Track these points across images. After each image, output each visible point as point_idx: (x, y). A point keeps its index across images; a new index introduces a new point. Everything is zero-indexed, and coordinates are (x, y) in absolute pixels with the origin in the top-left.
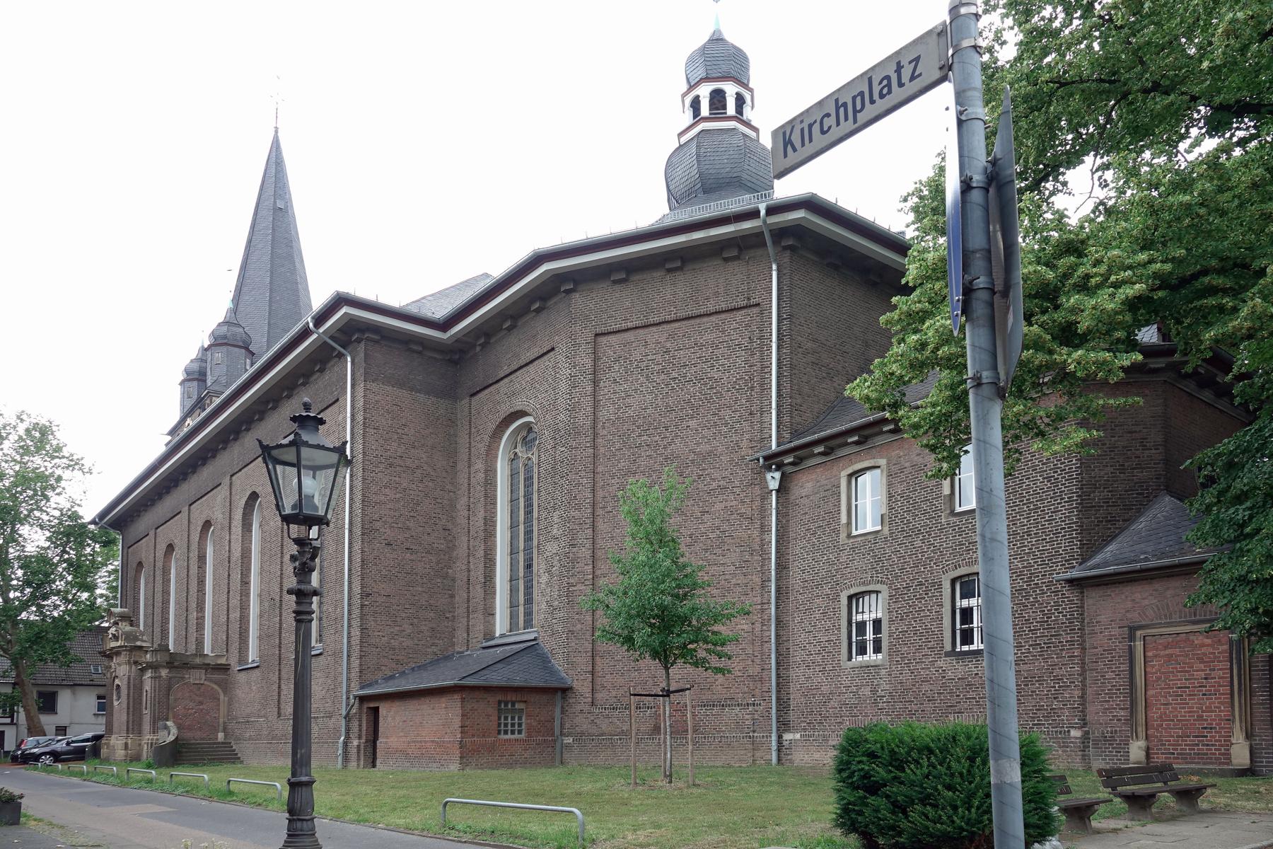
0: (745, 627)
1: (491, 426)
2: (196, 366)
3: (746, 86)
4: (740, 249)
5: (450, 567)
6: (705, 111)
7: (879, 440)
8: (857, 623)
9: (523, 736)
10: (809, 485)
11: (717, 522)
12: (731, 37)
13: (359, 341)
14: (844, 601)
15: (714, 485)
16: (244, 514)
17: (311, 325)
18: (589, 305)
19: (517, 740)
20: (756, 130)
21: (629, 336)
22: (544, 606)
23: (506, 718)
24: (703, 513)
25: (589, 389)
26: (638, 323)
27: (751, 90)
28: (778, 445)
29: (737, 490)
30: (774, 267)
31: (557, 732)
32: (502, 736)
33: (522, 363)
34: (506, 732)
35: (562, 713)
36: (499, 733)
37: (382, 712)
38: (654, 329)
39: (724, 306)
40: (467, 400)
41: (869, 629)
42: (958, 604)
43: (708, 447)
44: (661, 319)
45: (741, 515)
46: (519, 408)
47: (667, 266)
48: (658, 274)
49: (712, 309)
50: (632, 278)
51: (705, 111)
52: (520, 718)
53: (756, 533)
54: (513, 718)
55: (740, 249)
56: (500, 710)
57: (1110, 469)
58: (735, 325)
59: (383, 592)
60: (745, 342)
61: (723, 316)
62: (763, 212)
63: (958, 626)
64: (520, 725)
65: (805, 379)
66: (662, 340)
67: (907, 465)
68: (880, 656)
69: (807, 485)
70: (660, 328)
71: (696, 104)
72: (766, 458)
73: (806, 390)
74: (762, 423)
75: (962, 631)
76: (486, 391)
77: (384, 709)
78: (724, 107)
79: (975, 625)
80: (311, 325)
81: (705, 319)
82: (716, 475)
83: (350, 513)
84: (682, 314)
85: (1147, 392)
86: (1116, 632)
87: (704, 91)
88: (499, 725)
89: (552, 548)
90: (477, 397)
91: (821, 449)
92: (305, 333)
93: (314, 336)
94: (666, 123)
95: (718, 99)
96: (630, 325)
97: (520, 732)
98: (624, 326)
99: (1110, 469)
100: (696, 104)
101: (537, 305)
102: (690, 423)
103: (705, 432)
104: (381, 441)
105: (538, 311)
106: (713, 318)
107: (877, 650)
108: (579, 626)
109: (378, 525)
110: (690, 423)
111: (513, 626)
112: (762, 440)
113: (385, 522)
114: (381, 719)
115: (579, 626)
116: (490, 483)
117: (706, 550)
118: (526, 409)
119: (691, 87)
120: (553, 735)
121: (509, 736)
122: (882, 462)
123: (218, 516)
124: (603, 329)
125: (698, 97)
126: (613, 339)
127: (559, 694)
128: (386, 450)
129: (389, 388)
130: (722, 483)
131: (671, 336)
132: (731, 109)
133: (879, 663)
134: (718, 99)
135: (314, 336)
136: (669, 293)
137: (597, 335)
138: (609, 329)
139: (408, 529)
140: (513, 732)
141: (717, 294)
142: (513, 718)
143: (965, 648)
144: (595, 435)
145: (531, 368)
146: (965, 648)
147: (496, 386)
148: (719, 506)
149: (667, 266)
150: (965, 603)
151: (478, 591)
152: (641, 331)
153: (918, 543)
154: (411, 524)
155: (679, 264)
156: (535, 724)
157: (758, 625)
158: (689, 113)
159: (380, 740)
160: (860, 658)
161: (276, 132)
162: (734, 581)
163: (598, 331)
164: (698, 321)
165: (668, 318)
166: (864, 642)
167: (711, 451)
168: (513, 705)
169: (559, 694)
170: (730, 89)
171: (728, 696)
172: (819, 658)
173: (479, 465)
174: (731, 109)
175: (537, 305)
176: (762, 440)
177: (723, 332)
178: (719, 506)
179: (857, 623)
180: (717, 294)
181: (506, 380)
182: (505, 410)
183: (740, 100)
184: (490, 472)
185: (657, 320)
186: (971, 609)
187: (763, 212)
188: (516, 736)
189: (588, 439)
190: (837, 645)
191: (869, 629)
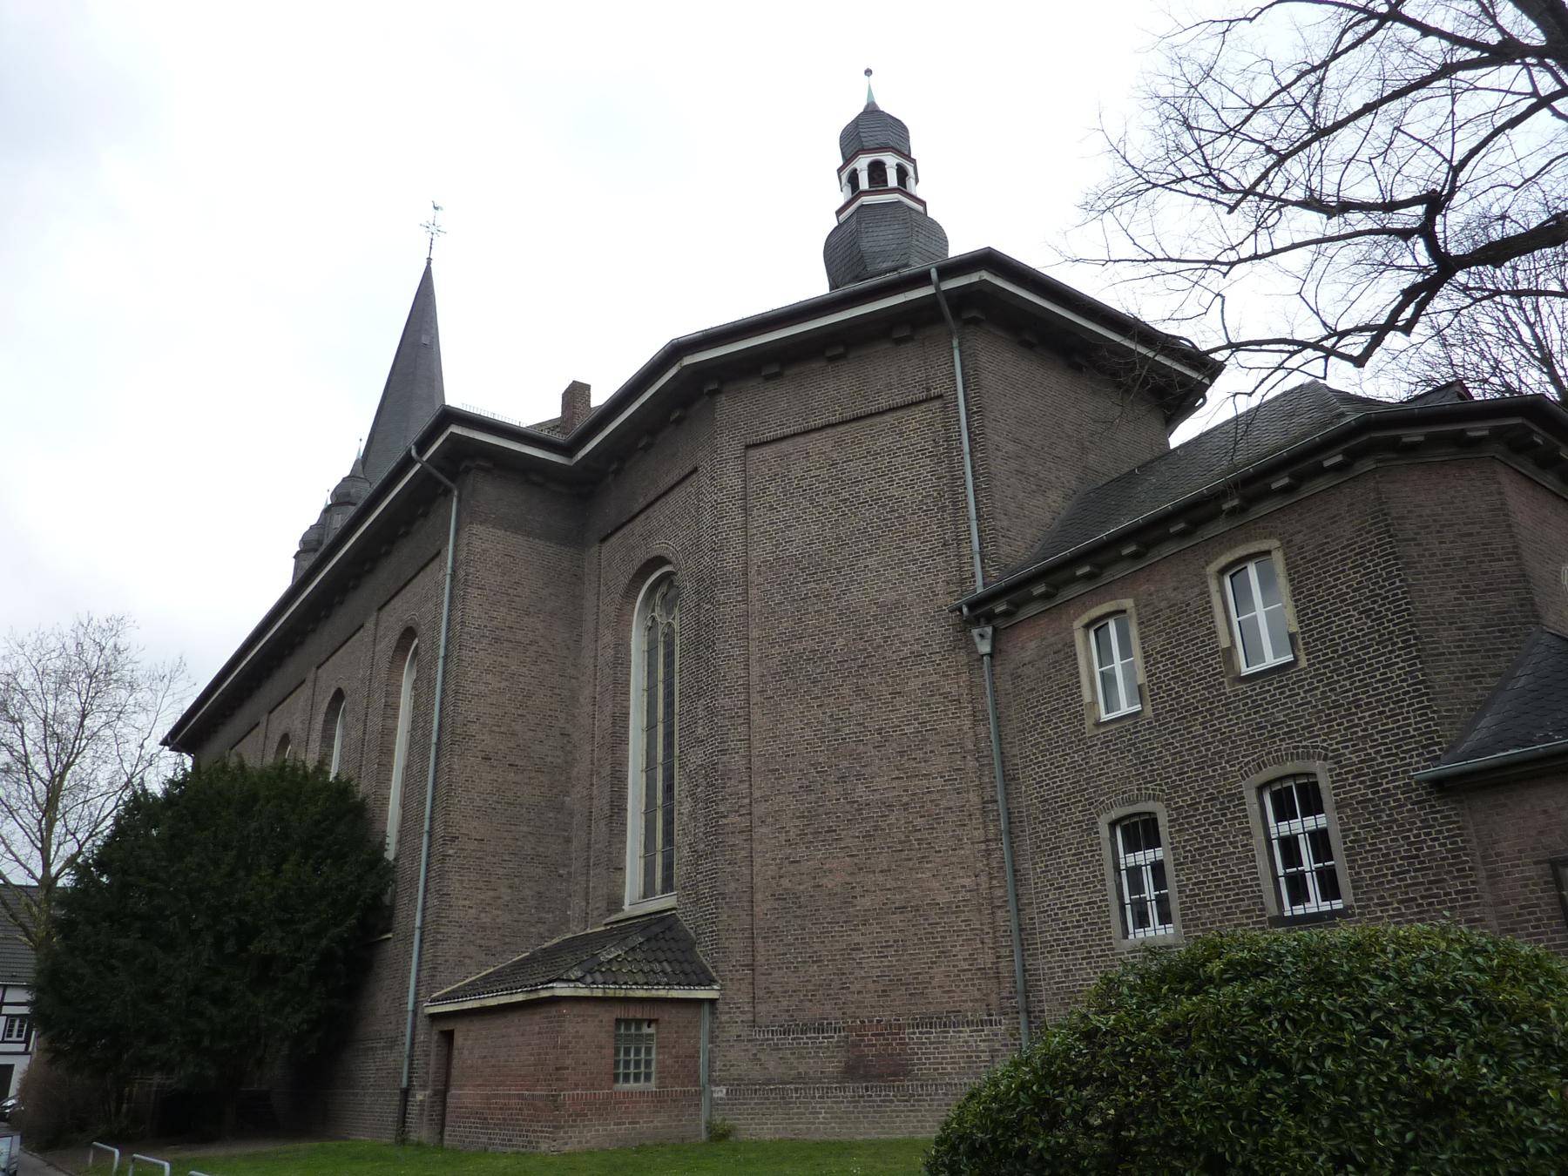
0: (966, 882)
1: (624, 581)
2: (314, 537)
3: (908, 157)
4: (913, 324)
5: (567, 794)
6: (864, 183)
7: (1119, 571)
8: (1128, 869)
9: (652, 1086)
10: (1033, 645)
11: (914, 708)
12: (884, 106)
13: (467, 471)
14: (1104, 832)
15: (906, 651)
16: (324, 730)
17: (413, 453)
18: (740, 412)
19: (642, 1093)
20: (923, 203)
21: (785, 446)
22: (686, 852)
23: (627, 1052)
24: (895, 694)
25: (739, 519)
26: (796, 429)
27: (913, 161)
28: (985, 585)
29: (937, 658)
30: (955, 343)
31: (703, 1078)
32: (621, 1086)
33: (661, 490)
34: (626, 1078)
35: (713, 1039)
36: (616, 1079)
37: (458, 1040)
38: (816, 435)
39: (899, 401)
40: (595, 549)
41: (1148, 879)
42: (1273, 831)
43: (894, 596)
44: (824, 422)
45: (945, 695)
46: (655, 553)
47: (829, 354)
48: (816, 365)
49: (885, 405)
50: (787, 372)
51: (864, 183)
52: (648, 1051)
53: (968, 723)
54: (638, 1052)
55: (913, 324)
56: (617, 1037)
57: (1452, 594)
58: (914, 425)
59: (474, 835)
60: (929, 446)
61: (899, 414)
62: (934, 275)
63: (1281, 871)
64: (648, 1063)
65: (1009, 492)
66: (828, 448)
67: (1163, 604)
68: (1170, 928)
69: (1028, 646)
70: (824, 434)
71: (853, 179)
72: (972, 606)
73: (1012, 507)
74: (959, 556)
75: (1288, 877)
76: (619, 534)
77: (461, 1031)
78: (885, 181)
79: (1306, 867)
80: (413, 453)
81: (878, 419)
82: (908, 636)
83: (441, 711)
84: (848, 415)
85: (1473, 474)
86: (1531, 872)
87: (862, 163)
88: (617, 1064)
89: (697, 757)
90: (608, 543)
91: (1039, 589)
92: (407, 462)
93: (418, 466)
94: (821, 202)
95: (877, 170)
96: (787, 431)
97: (648, 1077)
98: (779, 433)
99: (1452, 594)
100: (853, 179)
101: (677, 414)
102: (869, 562)
103: (889, 574)
104: (487, 606)
105: (679, 421)
106: (887, 417)
107: (1165, 918)
108: (733, 885)
109: (473, 728)
110: (869, 562)
111: (648, 892)
112: (962, 581)
113: (484, 725)
114: (456, 1052)
115: (733, 885)
116: (621, 662)
117: (902, 754)
118: (664, 553)
119: (848, 160)
120: (697, 1082)
121: (632, 1085)
122: (1128, 603)
123: (296, 726)
124: (754, 439)
125: (855, 170)
126: (767, 451)
127: (706, 1008)
128: (492, 618)
129: (501, 533)
130: (916, 647)
131: (838, 444)
132: (892, 181)
133: (1170, 941)
134: (877, 170)
135: (418, 466)
136: (832, 390)
137: (748, 447)
138: (764, 438)
139: (514, 734)
140: (637, 1079)
141: (889, 386)
142: (638, 1052)
143: (1299, 910)
144: (747, 583)
145: (671, 498)
146: (1299, 910)
147: (630, 526)
148: (914, 684)
149: (829, 354)
150: (1284, 828)
151: (600, 830)
152: (801, 440)
153: (1197, 729)
154: (518, 727)
155: (841, 350)
156: (669, 1062)
157: (984, 878)
158: (848, 189)
159: (453, 1092)
160: (1140, 933)
161: (429, 260)
162: (944, 803)
163: (749, 441)
164: (869, 422)
165: (833, 419)
166: (1143, 902)
167: (898, 601)
168: (638, 1028)
169: (706, 1008)
170: (891, 161)
171: (948, 1007)
172: (1079, 935)
173: (608, 637)
174: (892, 181)
175: (677, 414)
176: (962, 581)
177: (901, 434)
178: (914, 684)
179: (1128, 869)
180: (889, 386)
181: (642, 517)
182: (642, 556)
183: (902, 173)
184: (622, 646)
185: (819, 423)
186: (1295, 838)
187: (934, 275)
188: (641, 1085)
189: (740, 590)
190: (1103, 911)
191: (1148, 879)
